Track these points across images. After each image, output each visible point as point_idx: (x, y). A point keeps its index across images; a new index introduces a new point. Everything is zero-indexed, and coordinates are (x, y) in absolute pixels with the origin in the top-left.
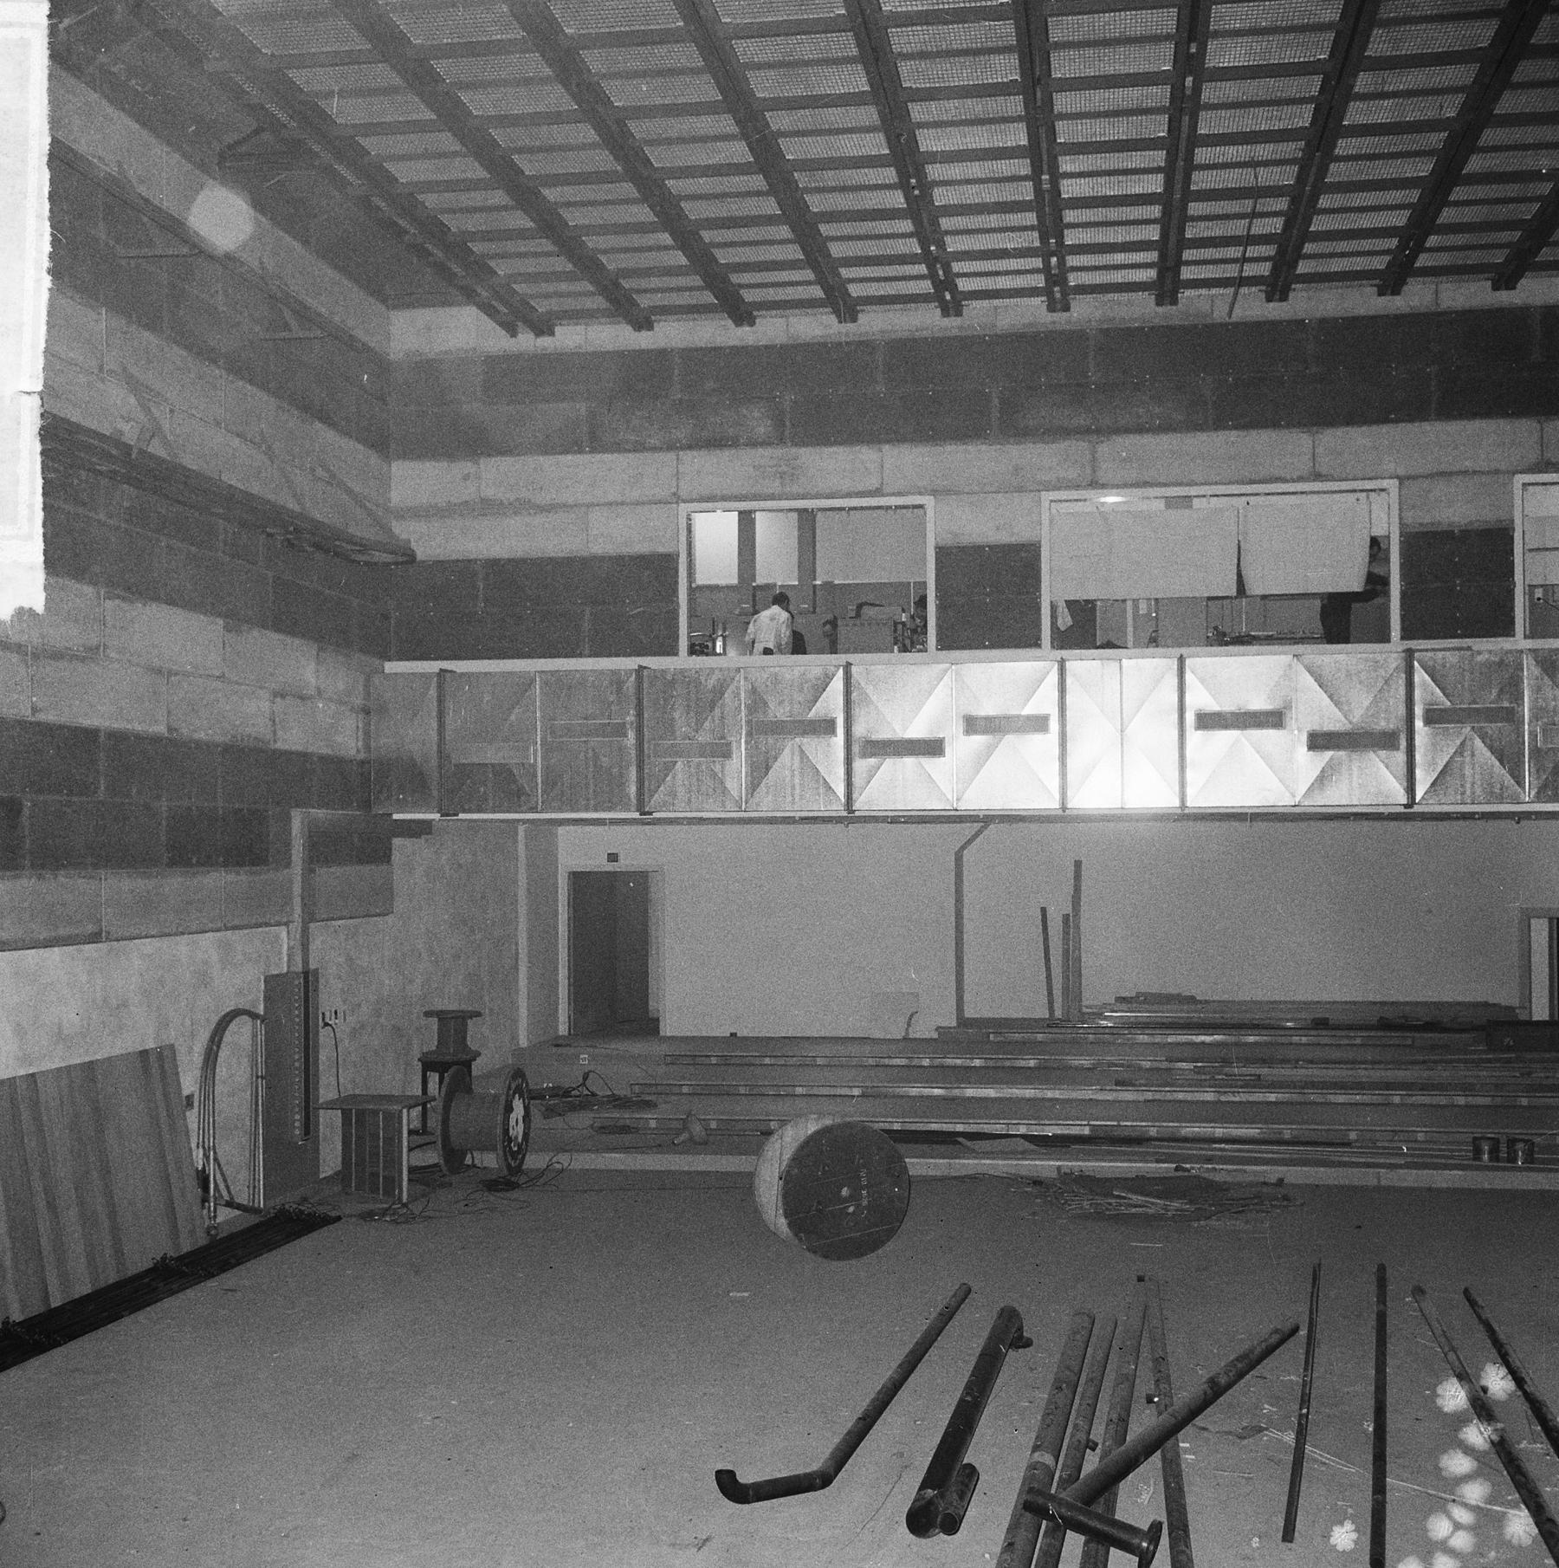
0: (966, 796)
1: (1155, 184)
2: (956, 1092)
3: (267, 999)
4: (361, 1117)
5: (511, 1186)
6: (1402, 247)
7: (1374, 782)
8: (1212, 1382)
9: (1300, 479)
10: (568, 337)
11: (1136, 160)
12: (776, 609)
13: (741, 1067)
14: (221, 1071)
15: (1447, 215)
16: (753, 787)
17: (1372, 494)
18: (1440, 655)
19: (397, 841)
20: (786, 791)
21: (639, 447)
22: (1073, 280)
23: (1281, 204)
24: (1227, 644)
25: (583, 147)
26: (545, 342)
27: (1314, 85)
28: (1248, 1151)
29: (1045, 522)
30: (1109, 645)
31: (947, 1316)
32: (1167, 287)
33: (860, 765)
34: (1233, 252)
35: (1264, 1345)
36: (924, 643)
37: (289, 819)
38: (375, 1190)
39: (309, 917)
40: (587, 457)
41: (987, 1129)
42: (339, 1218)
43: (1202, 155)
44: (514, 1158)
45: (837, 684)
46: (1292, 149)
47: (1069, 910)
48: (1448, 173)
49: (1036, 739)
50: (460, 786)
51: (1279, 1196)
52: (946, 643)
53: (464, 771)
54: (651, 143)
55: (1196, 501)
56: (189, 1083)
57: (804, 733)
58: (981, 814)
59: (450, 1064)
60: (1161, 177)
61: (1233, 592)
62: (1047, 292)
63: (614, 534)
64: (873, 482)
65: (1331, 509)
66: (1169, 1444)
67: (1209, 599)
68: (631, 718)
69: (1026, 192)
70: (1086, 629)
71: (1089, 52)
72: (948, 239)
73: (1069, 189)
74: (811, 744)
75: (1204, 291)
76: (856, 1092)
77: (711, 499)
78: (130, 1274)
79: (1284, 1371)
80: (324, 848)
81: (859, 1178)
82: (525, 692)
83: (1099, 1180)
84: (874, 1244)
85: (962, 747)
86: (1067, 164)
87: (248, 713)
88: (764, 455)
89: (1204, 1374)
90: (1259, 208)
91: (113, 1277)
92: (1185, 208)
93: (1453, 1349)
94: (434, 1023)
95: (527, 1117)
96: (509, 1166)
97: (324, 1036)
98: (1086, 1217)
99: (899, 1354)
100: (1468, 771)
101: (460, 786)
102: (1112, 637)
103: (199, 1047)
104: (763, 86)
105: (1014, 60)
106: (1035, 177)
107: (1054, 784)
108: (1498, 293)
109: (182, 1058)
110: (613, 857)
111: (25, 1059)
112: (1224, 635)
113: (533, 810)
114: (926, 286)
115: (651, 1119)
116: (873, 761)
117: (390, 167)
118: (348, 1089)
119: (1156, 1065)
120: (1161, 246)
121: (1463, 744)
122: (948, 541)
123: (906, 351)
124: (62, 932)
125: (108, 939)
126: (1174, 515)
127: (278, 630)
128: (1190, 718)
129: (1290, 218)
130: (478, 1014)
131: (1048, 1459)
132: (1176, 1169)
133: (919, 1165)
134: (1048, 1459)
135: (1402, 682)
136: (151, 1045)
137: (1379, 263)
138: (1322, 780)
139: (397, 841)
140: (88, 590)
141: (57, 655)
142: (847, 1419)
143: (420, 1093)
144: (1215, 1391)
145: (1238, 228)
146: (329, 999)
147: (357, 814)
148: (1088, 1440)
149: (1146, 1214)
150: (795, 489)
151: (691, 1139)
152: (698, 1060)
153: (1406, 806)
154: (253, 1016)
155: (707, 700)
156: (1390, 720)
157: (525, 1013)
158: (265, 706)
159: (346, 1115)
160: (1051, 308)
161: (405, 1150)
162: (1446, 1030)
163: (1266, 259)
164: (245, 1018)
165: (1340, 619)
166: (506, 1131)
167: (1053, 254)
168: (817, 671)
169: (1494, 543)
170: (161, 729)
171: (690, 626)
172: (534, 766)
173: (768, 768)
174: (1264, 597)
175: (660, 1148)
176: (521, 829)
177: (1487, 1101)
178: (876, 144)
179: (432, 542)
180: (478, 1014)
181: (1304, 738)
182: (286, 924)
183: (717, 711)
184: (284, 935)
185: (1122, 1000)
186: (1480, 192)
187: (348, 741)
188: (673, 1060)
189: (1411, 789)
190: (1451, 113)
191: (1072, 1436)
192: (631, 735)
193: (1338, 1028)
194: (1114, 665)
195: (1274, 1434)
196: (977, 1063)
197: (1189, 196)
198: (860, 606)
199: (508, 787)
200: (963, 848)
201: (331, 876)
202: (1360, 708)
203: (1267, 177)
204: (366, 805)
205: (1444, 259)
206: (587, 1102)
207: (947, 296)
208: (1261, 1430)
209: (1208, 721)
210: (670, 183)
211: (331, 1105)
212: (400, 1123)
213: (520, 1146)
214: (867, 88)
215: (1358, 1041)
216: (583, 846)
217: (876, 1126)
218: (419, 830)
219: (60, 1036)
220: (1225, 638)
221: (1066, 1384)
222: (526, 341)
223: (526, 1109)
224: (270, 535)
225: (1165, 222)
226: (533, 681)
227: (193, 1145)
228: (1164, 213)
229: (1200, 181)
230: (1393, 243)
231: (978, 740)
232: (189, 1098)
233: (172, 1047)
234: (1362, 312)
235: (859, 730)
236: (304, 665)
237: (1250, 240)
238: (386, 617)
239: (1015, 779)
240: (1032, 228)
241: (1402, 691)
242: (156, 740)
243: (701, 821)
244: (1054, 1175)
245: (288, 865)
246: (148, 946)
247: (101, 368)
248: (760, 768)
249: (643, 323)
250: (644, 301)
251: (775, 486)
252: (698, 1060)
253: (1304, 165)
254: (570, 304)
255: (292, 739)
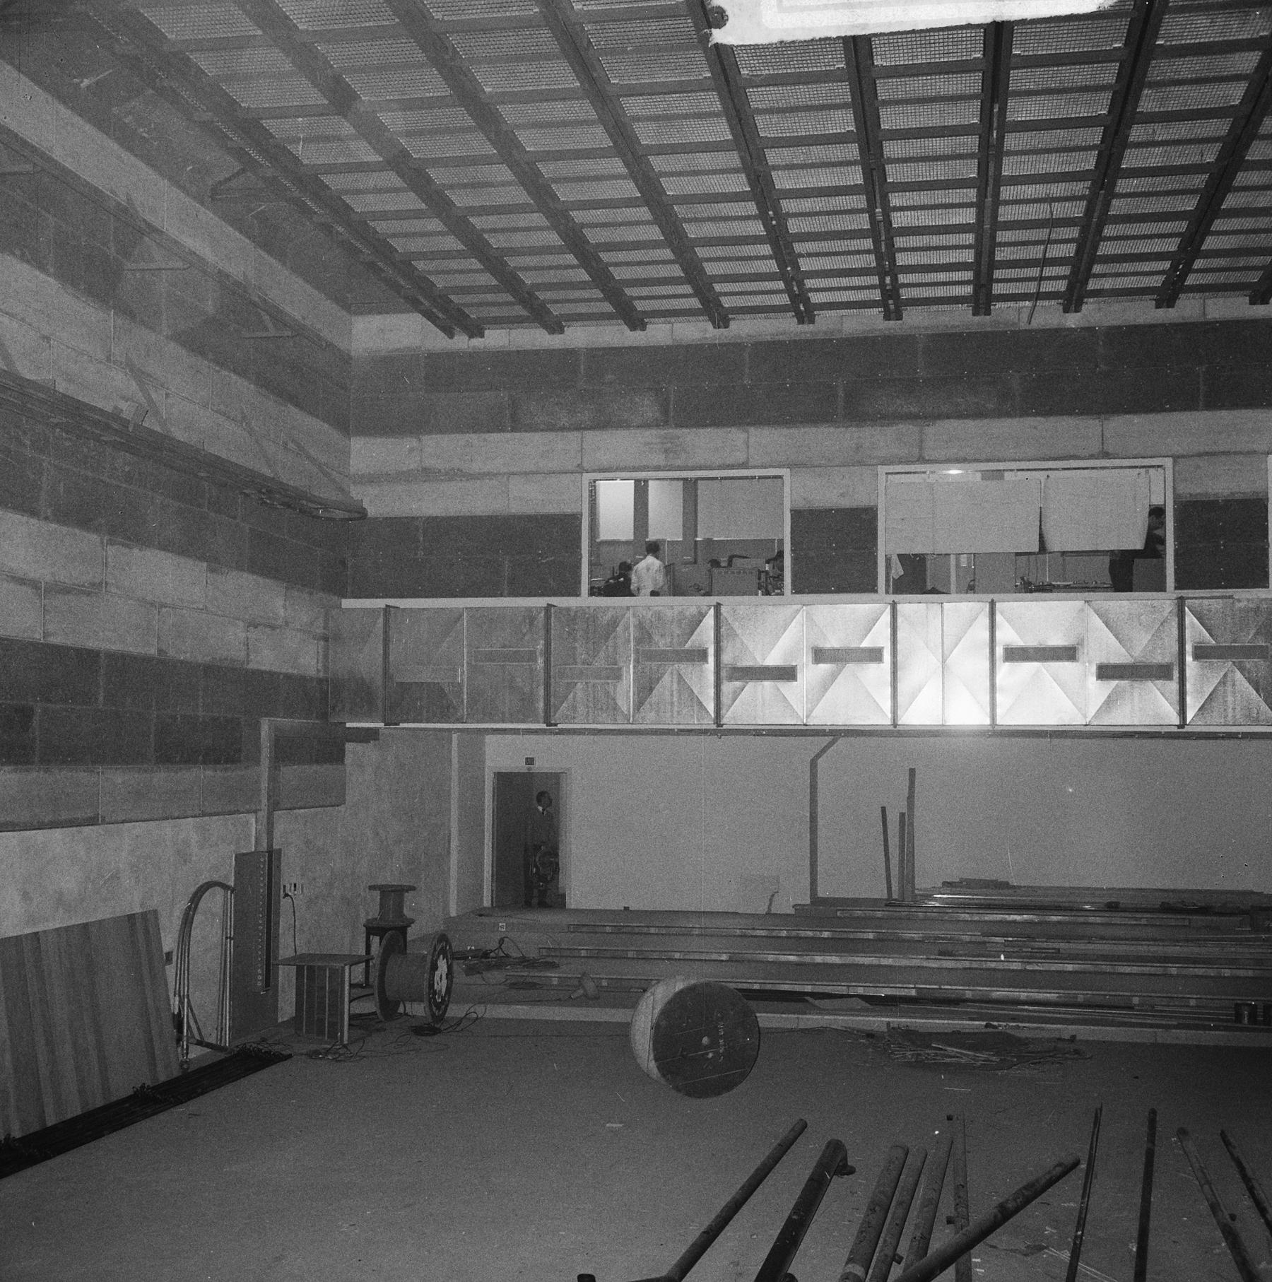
0: (814, 714)
1: (969, 216)
2: (807, 959)
3: (238, 873)
4: (311, 971)
5: (434, 1031)
6: (1174, 267)
7: (1152, 706)
8: (1002, 1206)
9: (1092, 457)
10: (495, 339)
11: (955, 196)
12: (650, 559)
13: (635, 934)
14: (196, 933)
15: (1210, 243)
16: (639, 704)
17: (1151, 470)
18: (1206, 602)
19: (349, 746)
20: (666, 710)
21: (552, 428)
22: (905, 294)
23: (1074, 232)
24: (1031, 592)
25: (503, 184)
26: (477, 342)
27: (1095, 136)
28: (1034, 1011)
29: (881, 488)
30: (934, 591)
31: (784, 1148)
32: (982, 300)
33: (727, 687)
34: (1034, 272)
35: (1048, 1177)
36: (781, 588)
37: (256, 727)
38: (321, 1032)
39: (274, 806)
40: (508, 435)
41: (828, 990)
42: (290, 1056)
43: (1007, 192)
44: (438, 1008)
45: (709, 621)
46: (1081, 188)
47: (905, 810)
48: (1209, 208)
49: (873, 666)
50: (402, 700)
51: (1069, 1051)
52: (798, 589)
53: (405, 687)
54: (556, 181)
55: (1006, 474)
56: (169, 942)
57: (680, 661)
58: (827, 728)
59: (390, 931)
60: (973, 210)
61: (1036, 549)
62: (882, 303)
63: (527, 498)
64: (740, 457)
65: (1114, 484)
66: (962, 1259)
67: (1017, 554)
68: (540, 646)
69: (863, 222)
70: (917, 577)
71: (910, 108)
72: (801, 261)
73: (899, 220)
74: (686, 669)
75: (1012, 304)
76: (724, 957)
77: (610, 470)
78: (114, 1099)
79: (1065, 1199)
80: (286, 751)
81: (716, 1028)
82: (446, 626)
83: (921, 1034)
84: (725, 1086)
85: (810, 673)
86: (896, 200)
87: (230, 642)
88: (651, 435)
89: (996, 1200)
90: (1053, 236)
91: (99, 1103)
92: (993, 237)
93: (1208, 1183)
94: (377, 894)
95: (450, 974)
96: (433, 1015)
97: (285, 903)
98: (909, 1065)
99: (742, 1179)
100: (1230, 699)
101: (402, 700)
102: (939, 588)
103: (178, 913)
104: (646, 135)
105: (849, 114)
106: (870, 211)
107: (887, 706)
108: (1255, 307)
109: (163, 921)
110: (530, 761)
111: (31, 920)
112: (1030, 584)
113: (460, 721)
114: (784, 299)
115: (554, 976)
116: (738, 684)
117: (348, 199)
118: (303, 950)
119: (973, 939)
120: (975, 266)
121: (1225, 675)
122: (801, 505)
123: (769, 349)
124: (64, 816)
125: (104, 822)
126: (992, 484)
127: (253, 573)
128: (999, 651)
129: (1081, 244)
130: (412, 888)
131: (858, 1270)
132: (987, 1026)
133: (768, 1019)
134: (858, 1270)
135: (1175, 624)
136: (138, 910)
137: (1157, 281)
138: (1109, 703)
139: (349, 746)
140: (94, 537)
141: (67, 591)
142: (694, 1232)
143: (364, 953)
144: (1004, 1215)
145: (1036, 252)
146: (290, 875)
147: (319, 722)
148: (895, 1255)
149: (959, 1063)
150: (678, 462)
151: (586, 995)
152: (597, 929)
153: (1179, 727)
154: (225, 887)
155: (601, 632)
156: (1165, 653)
157: (457, 886)
158: (242, 635)
159: (300, 970)
160: (887, 317)
161: (346, 999)
162: (1216, 914)
163: (1063, 277)
164: (218, 889)
165: (1125, 572)
166: (431, 986)
167: (887, 274)
168: (693, 610)
169: (1250, 512)
170: (153, 651)
171: (591, 572)
172: (460, 685)
173: (651, 690)
174: (1063, 553)
175: (559, 1002)
176: (455, 736)
177: (1250, 973)
178: (739, 183)
179: (379, 503)
180: (412, 888)
181: (1094, 669)
182: (255, 812)
183: (610, 643)
184: (253, 820)
185: (946, 884)
186: (1235, 223)
187: (309, 662)
188: (578, 928)
189: (1182, 711)
190: (1210, 158)
191: (882, 1251)
192: (540, 661)
193: (1125, 910)
194: (937, 607)
195: (1053, 1251)
196: (826, 935)
197: (997, 226)
198: (731, 558)
199: (439, 702)
200: (819, 756)
201: (290, 773)
202: (1140, 647)
203: (1060, 210)
204: (324, 716)
205: (1208, 279)
206: (502, 962)
207: (803, 309)
208: (1041, 1248)
209: (1014, 654)
210: (573, 214)
211: (287, 962)
212: (343, 978)
213: (443, 999)
214: (730, 137)
215: (1144, 922)
216: (504, 752)
217: (732, 986)
218: (369, 736)
219: (60, 899)
220: (1031, 587)
221: (879, 1207)
222: (461, 342)
223: (450, 967)
224: (247, 495)
225: (977, 247)
226: (461, 615)
227: (171, 995)
228: (976, 240)
229: (1006, 214)
230: (1166, 265)
231: (824, 668)
232: (169, 955)
233: (155, 911)
234: (1141, 321)
235: (726, 658)
236: (276, 601)
237: (1045, 262)
238: (343, 563)
239: (858, 700)
240: (868, 252)
241: (1175, 632)
242: (147, 659)
243: (600, 732)
244: (884, 1029)
245: (258, 763)
246: (139, 828)
247: (108, 359)
248: (646, 688)
249: (556, 327)
250: (556, 310)
251: (659, 459)
252: (597, 929)
253: (1091, 201)
254: (495, 312)
255: (266, 659)
